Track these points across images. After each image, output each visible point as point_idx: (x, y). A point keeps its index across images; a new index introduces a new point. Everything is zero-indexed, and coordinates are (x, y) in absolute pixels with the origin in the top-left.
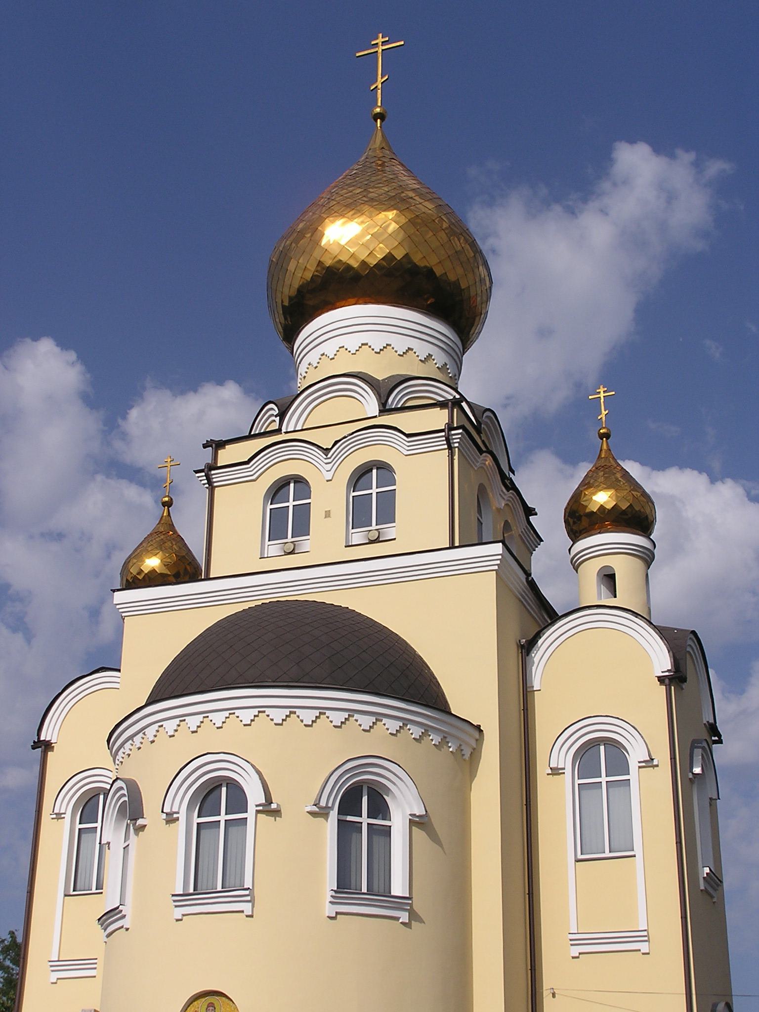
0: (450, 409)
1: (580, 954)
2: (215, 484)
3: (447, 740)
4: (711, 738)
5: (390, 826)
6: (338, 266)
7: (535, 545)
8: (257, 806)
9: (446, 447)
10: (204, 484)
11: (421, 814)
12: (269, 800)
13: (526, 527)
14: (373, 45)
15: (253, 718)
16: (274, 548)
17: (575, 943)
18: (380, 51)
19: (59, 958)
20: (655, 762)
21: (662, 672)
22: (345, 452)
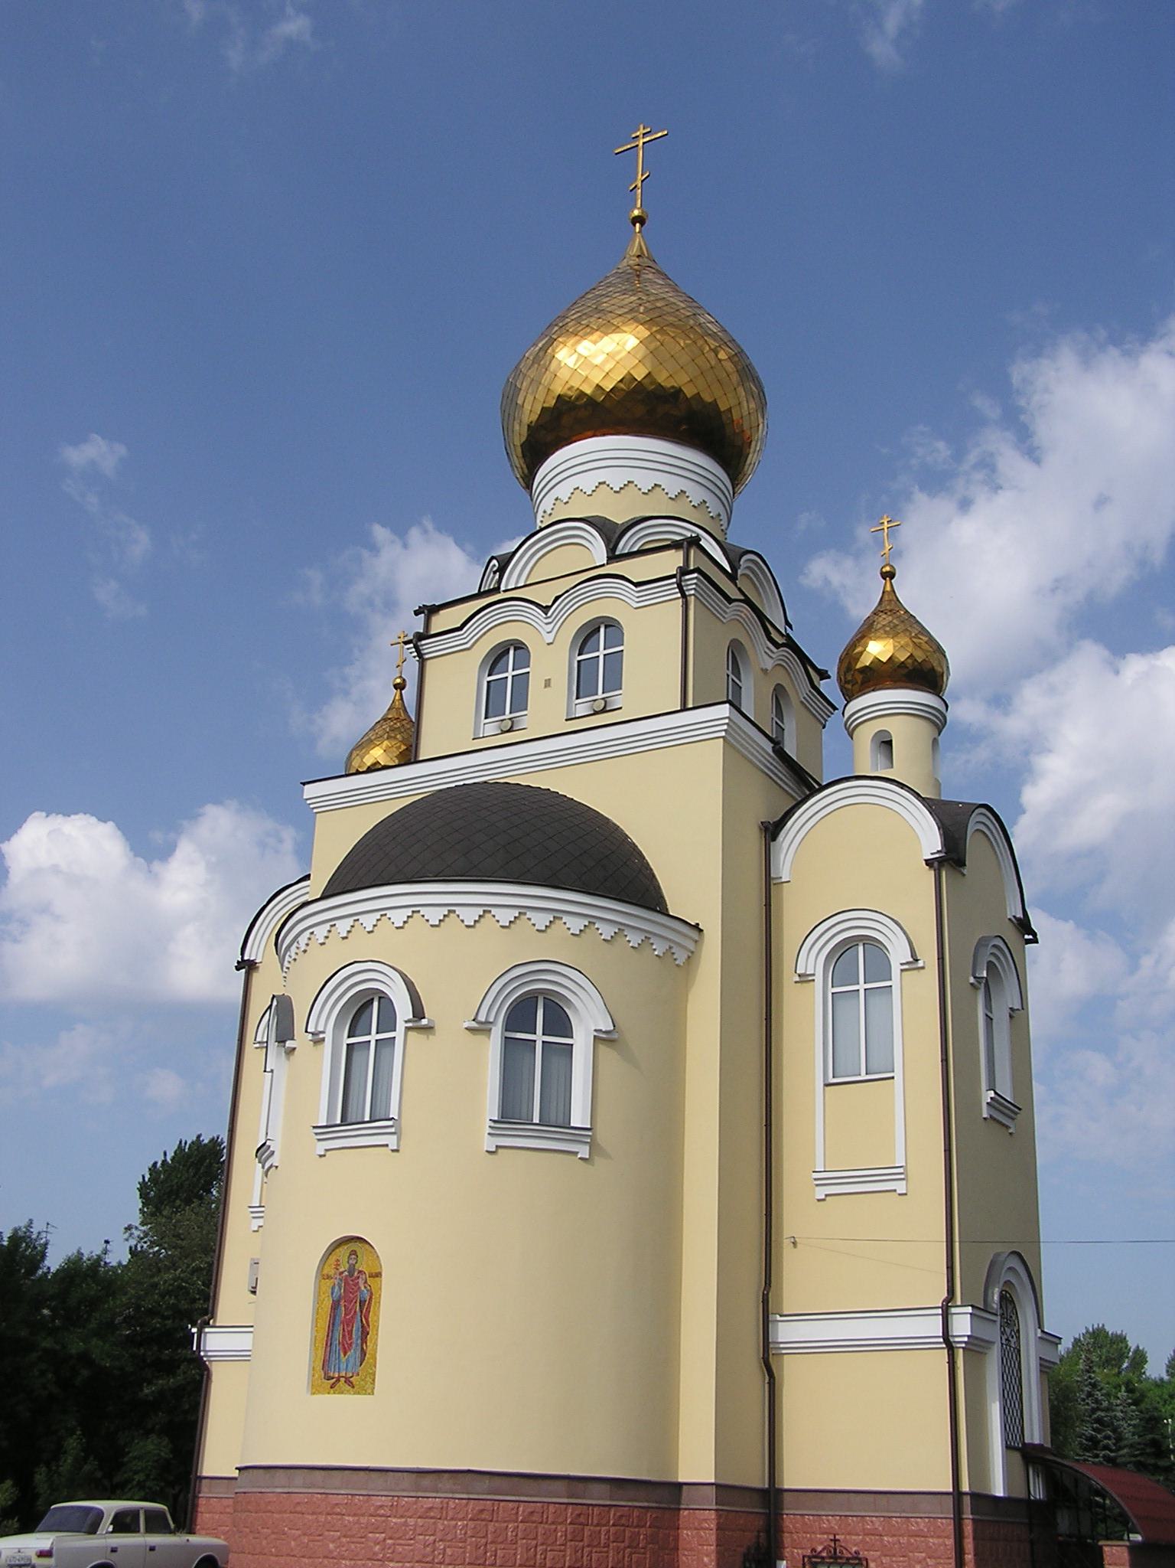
0: (685, 550)
1: (826, 1195)
2: (427, 656)
3: (651, 941)
4: (1024, 937)
5: (572, 1045)
6: (570, 393)
7: (826, 714)
8: (406, 1022)
9: (679, 595)
10: (415, 657)
11: (608, 1029)
13: (810, 691)
14: (634, 138)
15: (405, 919)
16: (490, 727)
17: (821, 1183)
18: (641, 144)
19: (260, 1202)
20: (920, 964)
21: (932, 854)
22: (569, 609)
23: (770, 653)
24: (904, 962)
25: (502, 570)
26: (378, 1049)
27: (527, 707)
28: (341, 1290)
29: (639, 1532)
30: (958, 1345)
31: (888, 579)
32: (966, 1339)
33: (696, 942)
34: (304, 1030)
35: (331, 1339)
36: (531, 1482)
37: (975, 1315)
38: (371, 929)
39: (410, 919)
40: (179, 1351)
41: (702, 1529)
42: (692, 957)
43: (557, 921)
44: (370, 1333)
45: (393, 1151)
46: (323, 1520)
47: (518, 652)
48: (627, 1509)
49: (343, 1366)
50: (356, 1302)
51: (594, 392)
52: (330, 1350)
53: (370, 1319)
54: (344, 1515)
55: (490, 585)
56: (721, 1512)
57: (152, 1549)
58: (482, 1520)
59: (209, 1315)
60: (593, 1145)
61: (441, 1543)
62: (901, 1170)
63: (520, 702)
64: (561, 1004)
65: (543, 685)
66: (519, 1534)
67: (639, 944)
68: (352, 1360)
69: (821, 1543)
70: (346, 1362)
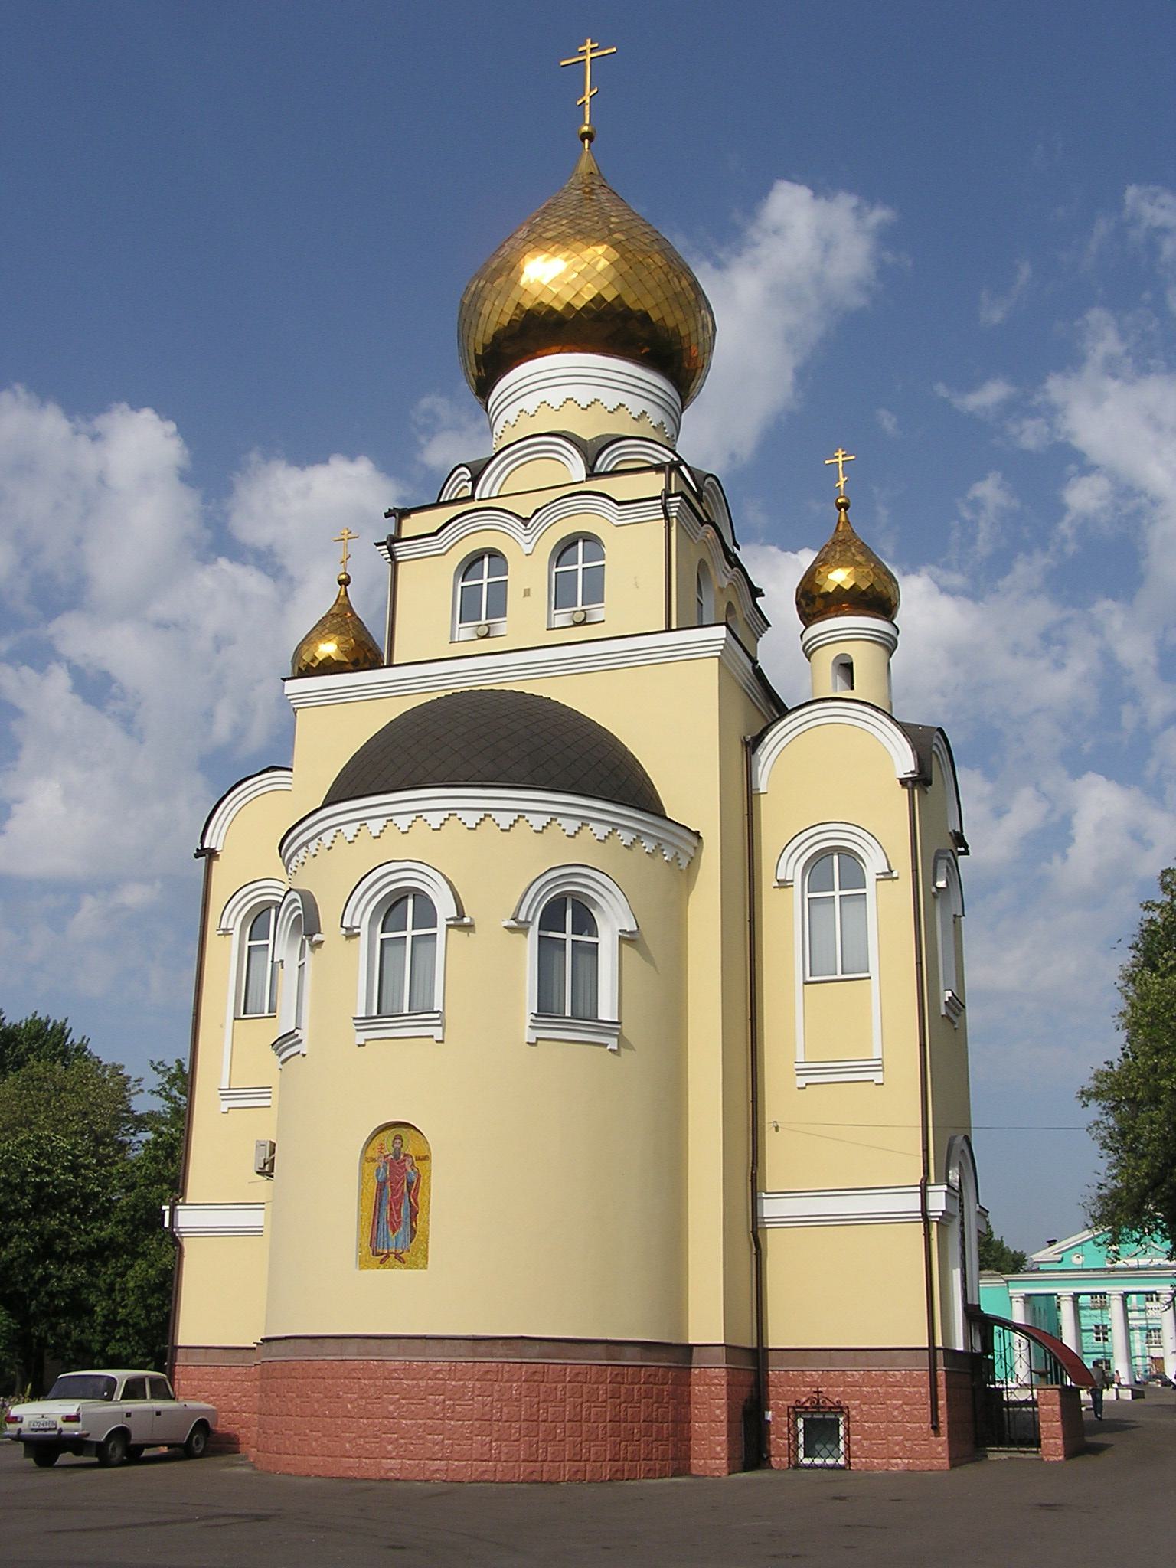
1: (807, 1084)
2: (399, 559)
9: (662, 516)
10: (386, 559)
11: (632, 929)
12: (461, 914)
14: (581, 52)
16: (466, 631)
17: (801, 1072)
19: (230, 1085)
20: (895, 875)
21: (905, 774)
23: (726, 572)
24: (880, 872)
25: (475, 480)
26: (414, 945)
27: (506, 613)
28: (386, 1172)
29: (598, 1387)
30: (933, 1219)
31: (843, 510)
32: (940, 1214)
33: (695, 848)
34: (339, 925)
35: (379, 1218)
36: (574, 1346)
37: (951, 1195)
38: (406, 830)
39: (447, 822)
40: (10, 1224)
41: (714, 1385)
42: (694, 862)
43: (584, 828)
44: (420, 1212)
45: (437, 1042)
46: (381, 1384)
47: (493, 559)
48: (653, 1368)
49: (392, 1243)
50: (403, 1184)
51: (564, 309)
52: (378, 1228)
53: (418, 1200)
54: (402, 1379)
55: (451, 496)
56: (729, 1370)
57: (158, 1413)
58: (534, 1382)
59: (180, 1194)
60: (621, 1039)
61: (498, 1403)
62: (880, 1062)
63: (498, 608)
64: (588, 906)
65: (523, 595)
66: (567, 1393)
67: (653, 850)
68: (401, 1238)
69: (805, 1396)
70: (395, 1240)
